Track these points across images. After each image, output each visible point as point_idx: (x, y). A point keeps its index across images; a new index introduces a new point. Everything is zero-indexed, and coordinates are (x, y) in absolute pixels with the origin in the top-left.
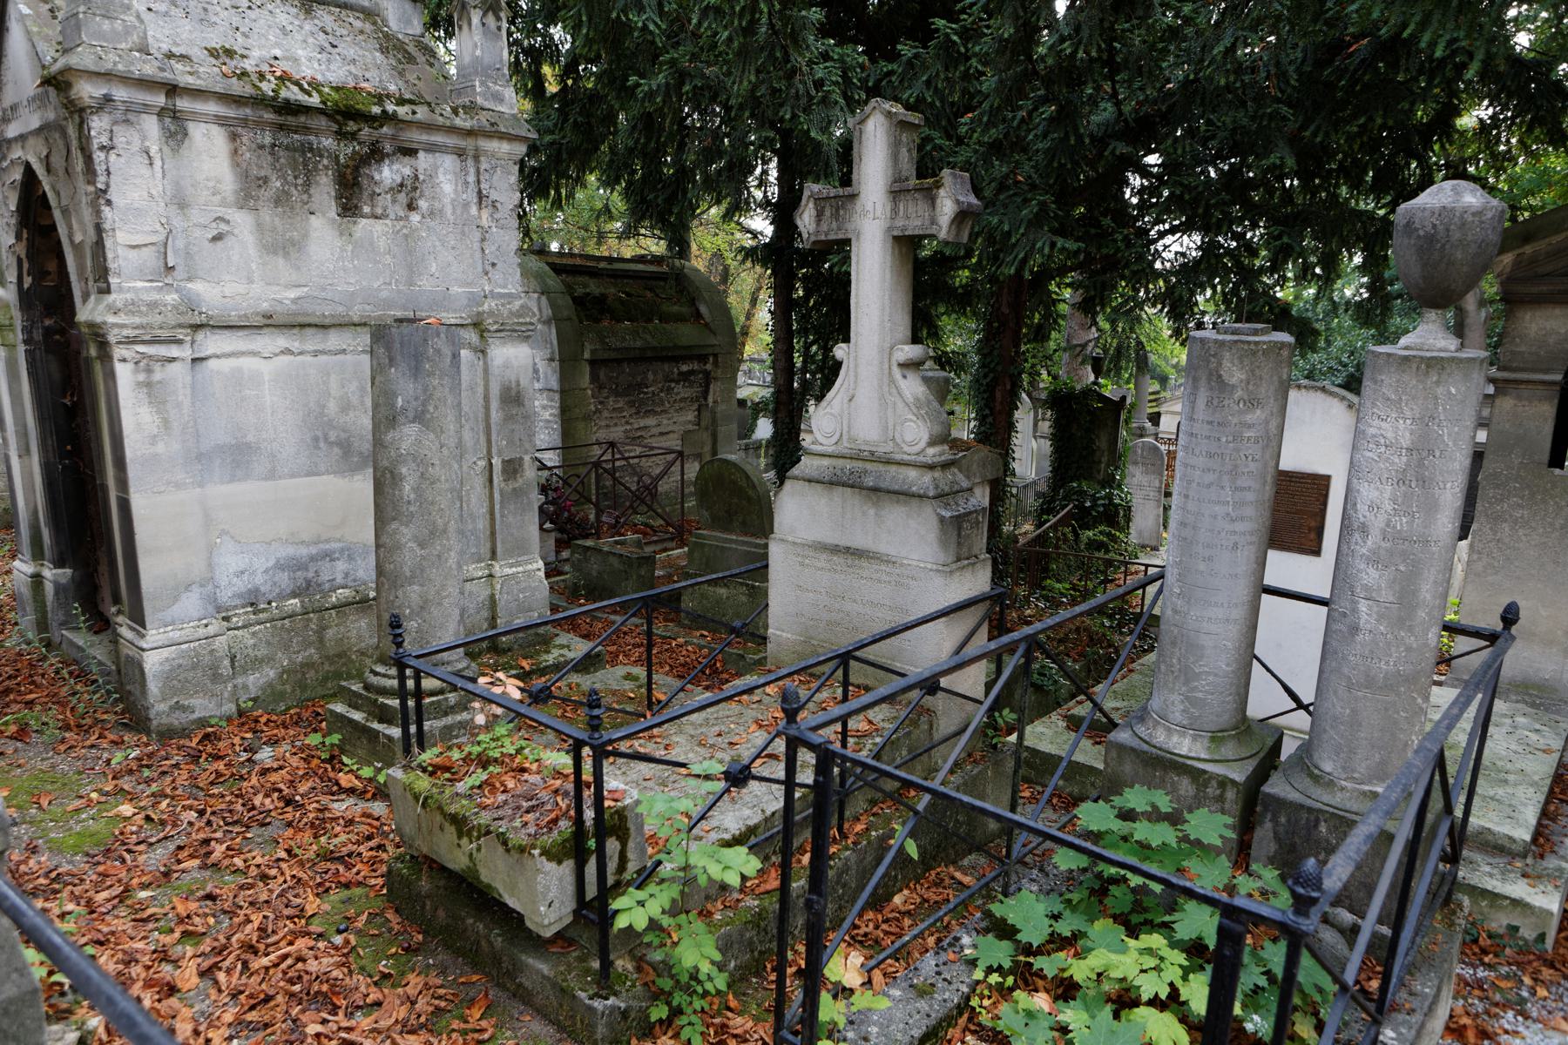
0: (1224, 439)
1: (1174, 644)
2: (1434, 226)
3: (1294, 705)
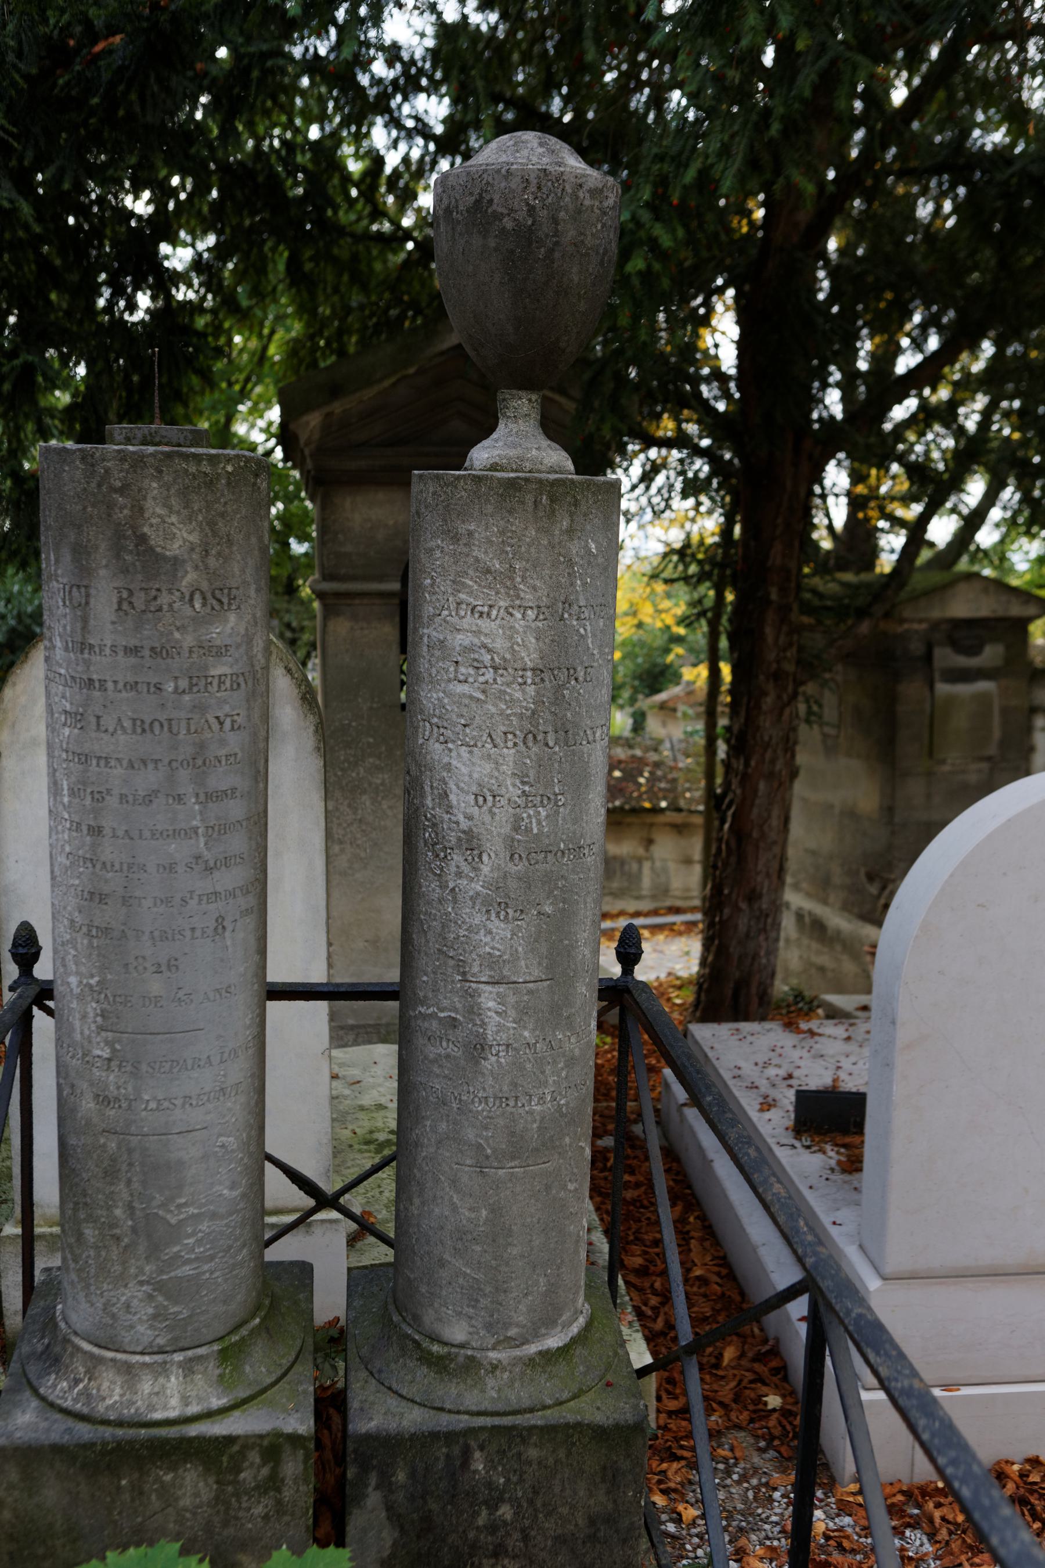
0: (170, 687)
1: (111, 1173)
2: (531, 209)
3: (311, 1202)
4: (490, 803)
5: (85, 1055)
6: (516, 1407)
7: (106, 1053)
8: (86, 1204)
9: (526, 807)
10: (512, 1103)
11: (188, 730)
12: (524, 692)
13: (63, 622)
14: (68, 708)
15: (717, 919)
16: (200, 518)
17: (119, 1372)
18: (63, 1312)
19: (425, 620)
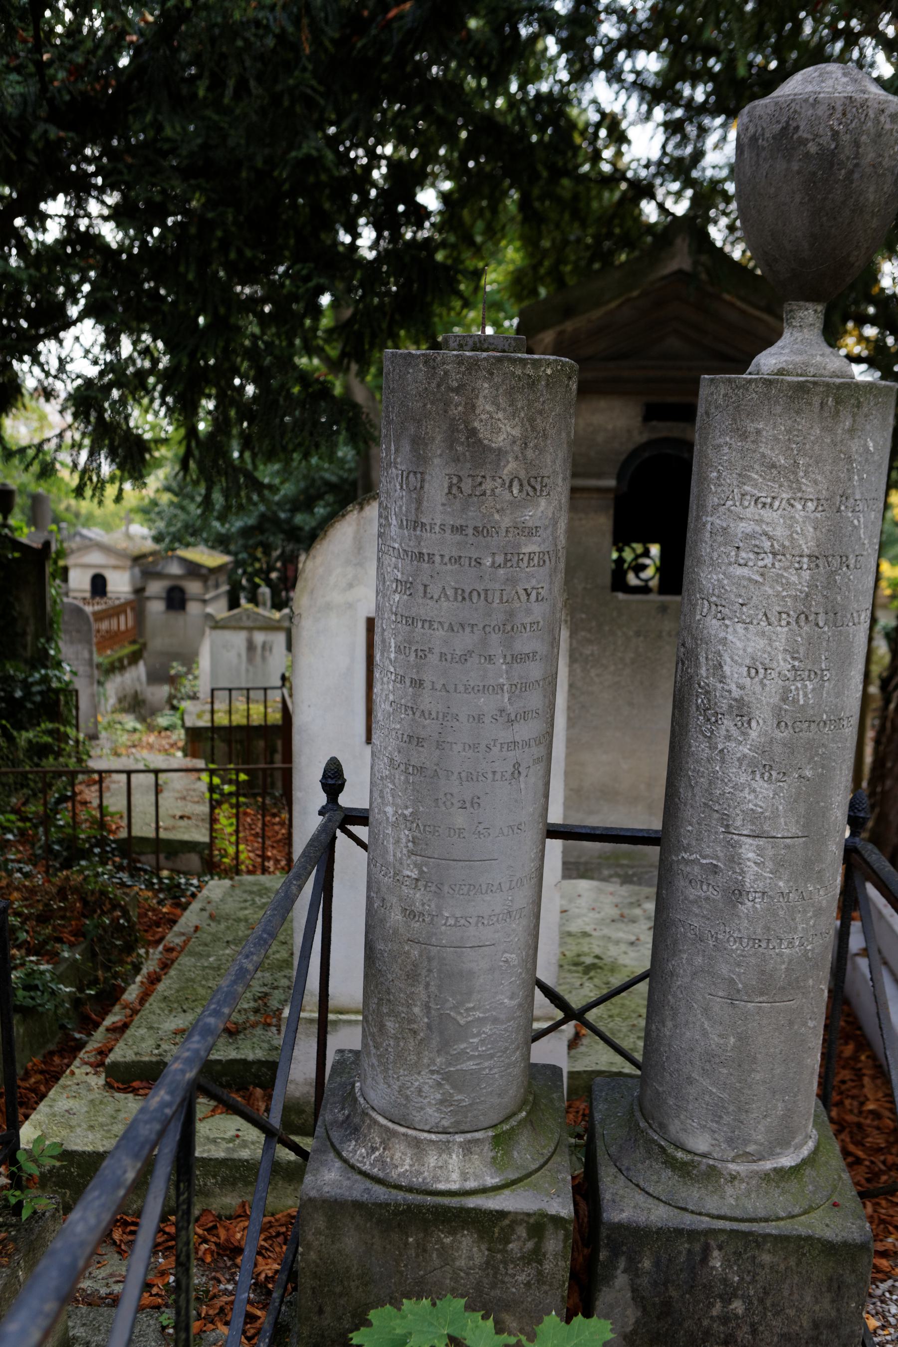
0: (488, 562)
1: (413, 976)
2: (835, 134)
3: (560, 1015)
4: (761, 676)
5: (396, 874)
6: (753, 1215)
7: (414, 874)
8: (389, 1000)
9: (795, 680)
10: (764, 944)
11: (501, 600)
12: (799, 576)
13: (399, 503)
14: (399, 577)
15: (879, 789)
16: (522, 415)
17: (409, 1145)
18: (361, 1089)
19: (709, 509)
